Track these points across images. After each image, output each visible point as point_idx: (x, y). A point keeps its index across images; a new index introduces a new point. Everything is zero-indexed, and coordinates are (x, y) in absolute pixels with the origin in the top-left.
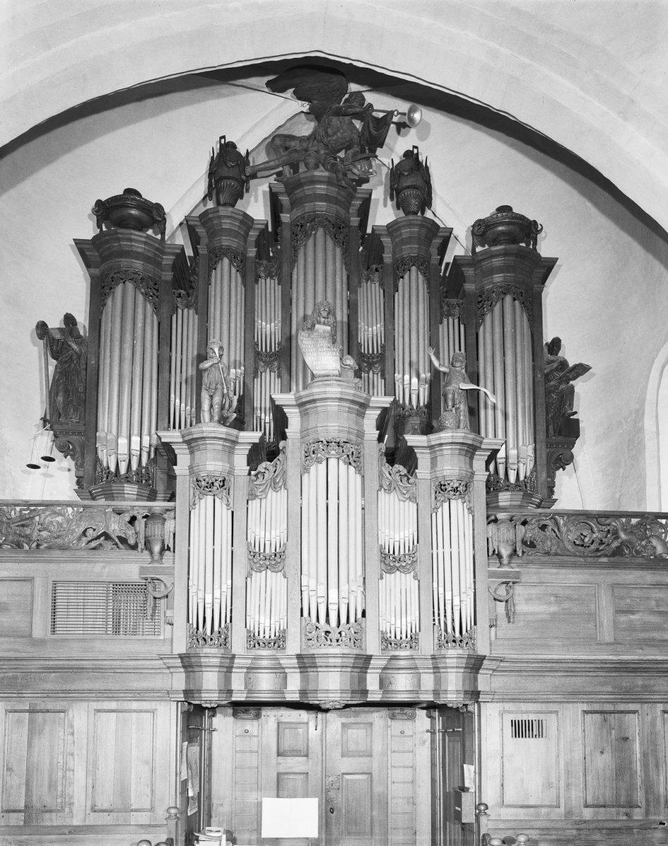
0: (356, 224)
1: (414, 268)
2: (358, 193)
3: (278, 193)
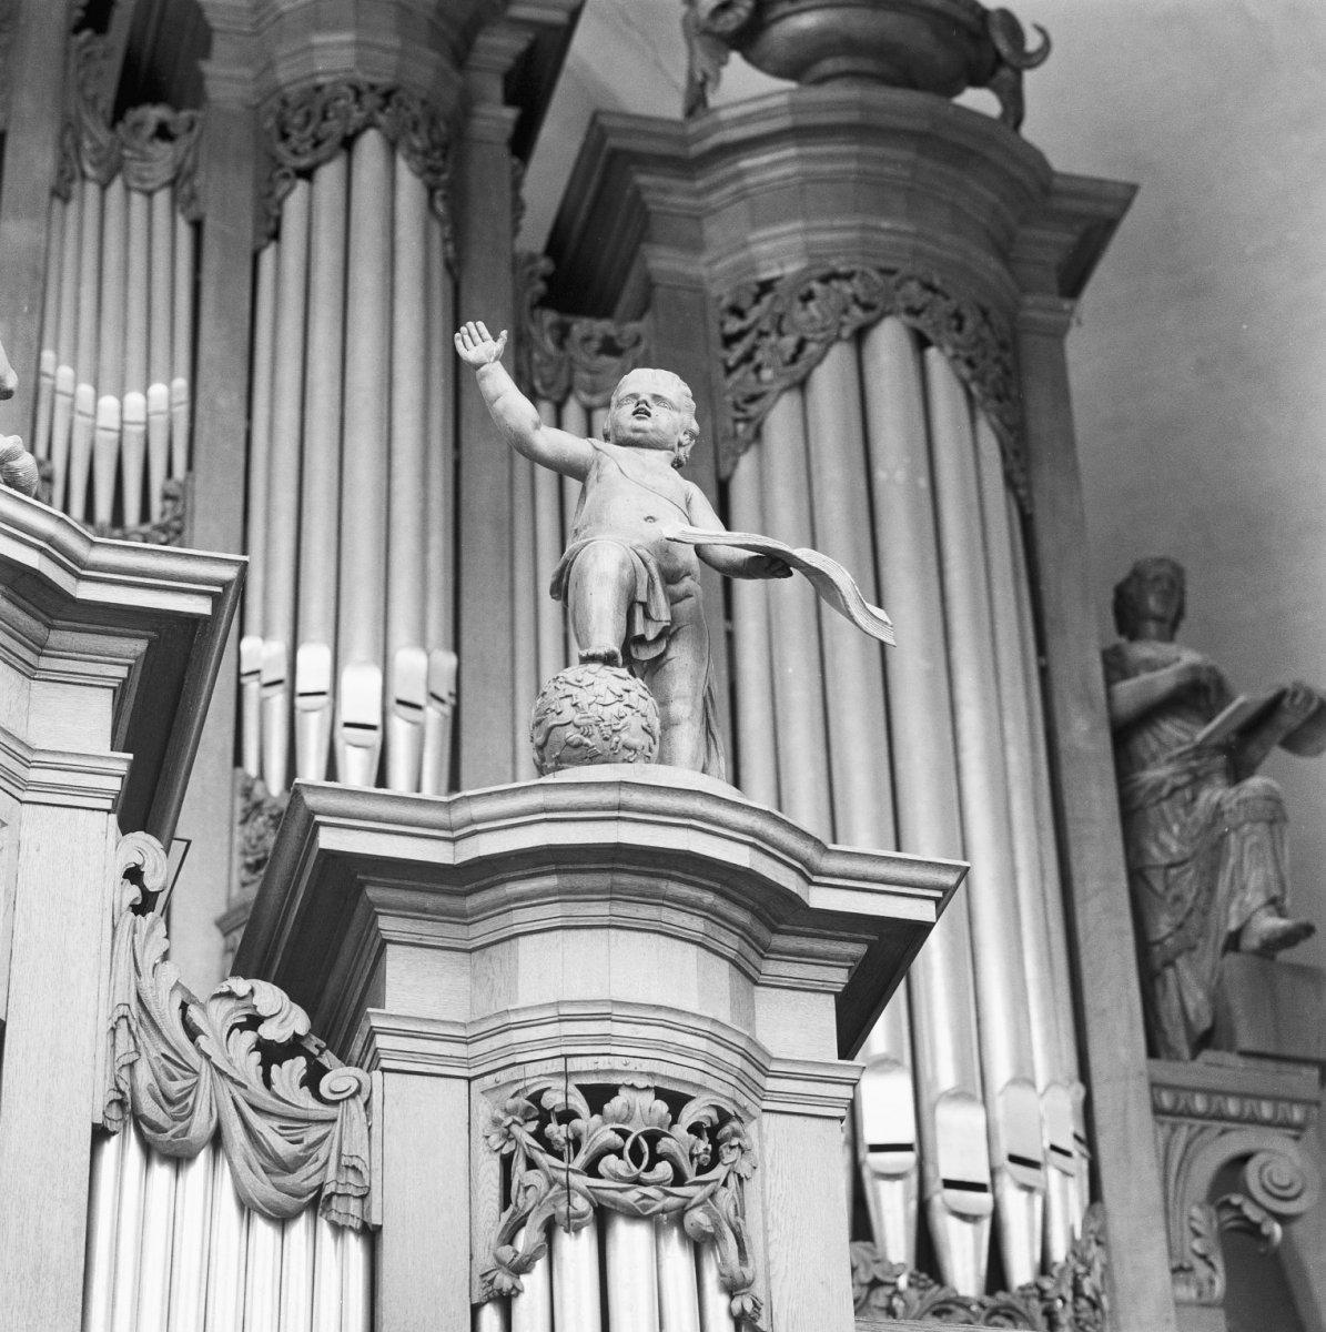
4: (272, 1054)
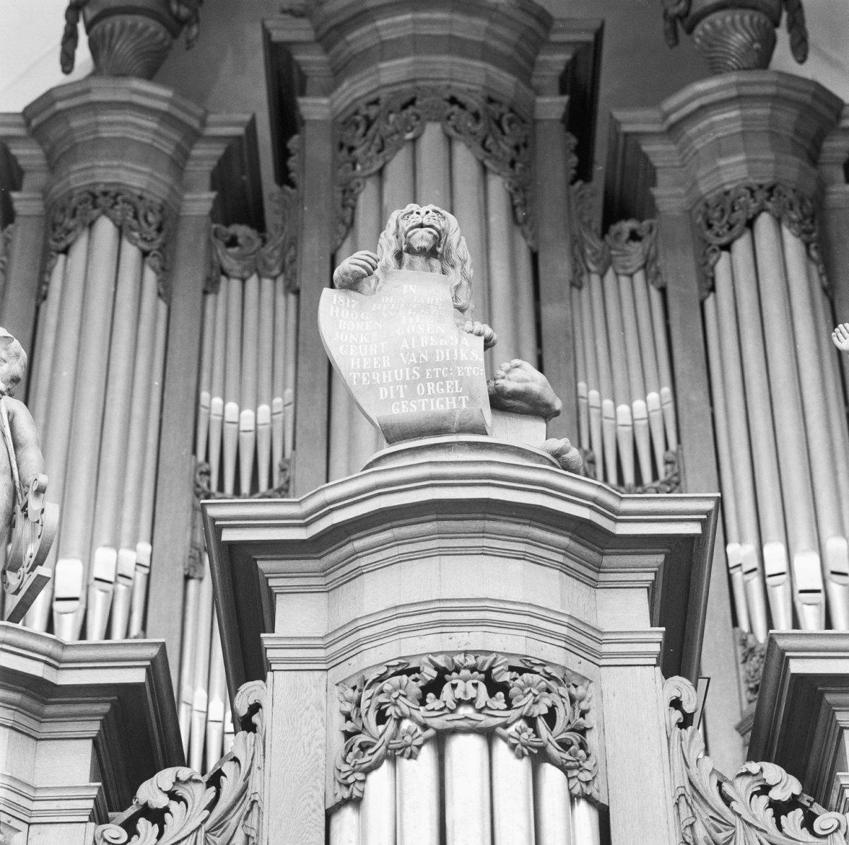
2: (558, 31)
3: (290, 43)
4: (779, 809)
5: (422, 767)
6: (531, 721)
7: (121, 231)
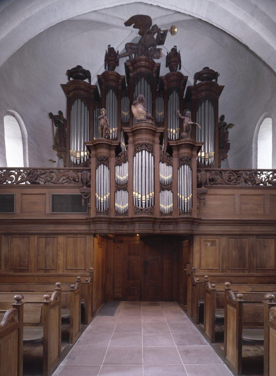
0: (155, 76)
1: (175, 91)
4: (168, 157)
5: (140, 153)
6: (149, 149)
7: (113, 91)
